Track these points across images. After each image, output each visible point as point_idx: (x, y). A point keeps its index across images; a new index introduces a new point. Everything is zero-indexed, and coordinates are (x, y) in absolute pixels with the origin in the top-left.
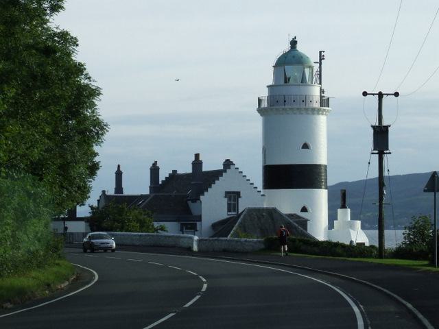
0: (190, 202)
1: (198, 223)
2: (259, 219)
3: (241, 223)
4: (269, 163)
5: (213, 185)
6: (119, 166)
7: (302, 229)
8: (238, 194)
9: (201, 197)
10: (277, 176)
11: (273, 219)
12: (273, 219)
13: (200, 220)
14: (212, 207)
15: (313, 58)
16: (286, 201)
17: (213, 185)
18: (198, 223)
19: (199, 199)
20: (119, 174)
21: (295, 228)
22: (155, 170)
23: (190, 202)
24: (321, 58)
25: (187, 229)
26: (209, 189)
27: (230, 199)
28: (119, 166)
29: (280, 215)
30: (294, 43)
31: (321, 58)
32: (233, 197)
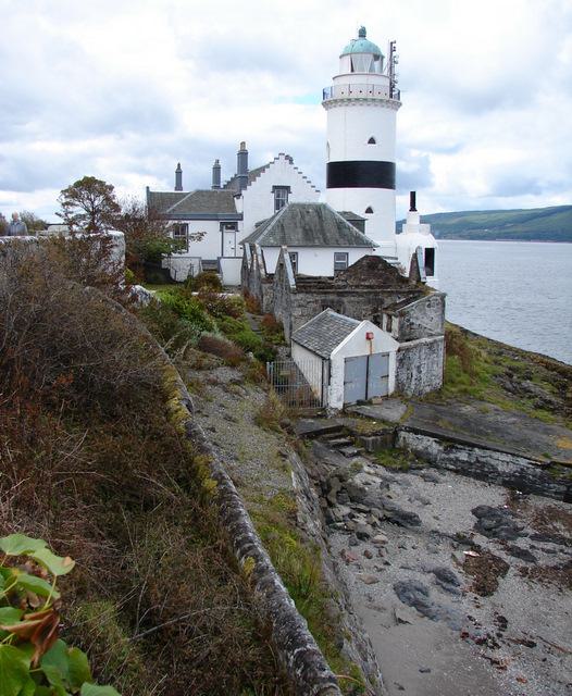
8: (287, 189)
9: (243, 192)
13: (242, 219)
14: (255, 205)
16: (347, 200)
20: (179, 173)
22: (217, 169)
24: (393, 50)
25: (227, 228)
31: (393, 50)
32: (281, 191)
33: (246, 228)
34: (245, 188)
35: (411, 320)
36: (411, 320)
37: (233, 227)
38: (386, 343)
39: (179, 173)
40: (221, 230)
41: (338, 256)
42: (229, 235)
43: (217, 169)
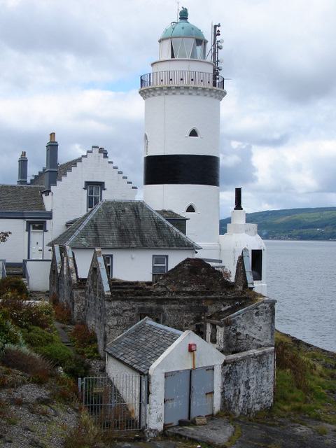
0: (44, 195)
1: (48, 222)
2: (118, 216)
3: (92, 220)
4: (151, 154)
5: (63, 178)
7: (178, 231)
8: (101, 185)
9: (53, 188)
10: (162, 169)
11: (137, 216)
12: (137, 216)
14: (66, 203)
16: (166, 198)
17: (63, 178)
18: (48, 221)
19: (50, 191)
21: (169, 228)
22: (23, 163)
23: (44, 195)
24: (217, 34)
25: (35, 228)
26: (58, 182)
27: (91, 192)
29: (150, 211)
30: (184, 15)
31: (217, 34)
32: (94, 188)
33: (55, 227)
34: (55, 184)
35: (238, 330)
36: (238, 330)
37: (41, 226)
38: (211, 355)
40: (28, 230)
41: (157, 259)
42: (37, 236)
43: (23, 163)
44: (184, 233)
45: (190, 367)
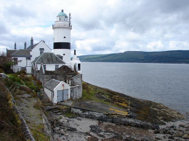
6: (15, 43)
8: (43, 49)
9: (32, 50)
14: (35, 53)
15: (68, 16)
20: (15, 45)
22: (25, 44)
24: (70, 15)
28: (15, 43)
31: (70, 15)
32: (42, 50)
33: (33, 59)
34: (33, 49)
39: (15, 45)
40: (26, 59)
42: (28, 61)
43: (25, 44)
44: (62, 60)
45: (63, 89)
